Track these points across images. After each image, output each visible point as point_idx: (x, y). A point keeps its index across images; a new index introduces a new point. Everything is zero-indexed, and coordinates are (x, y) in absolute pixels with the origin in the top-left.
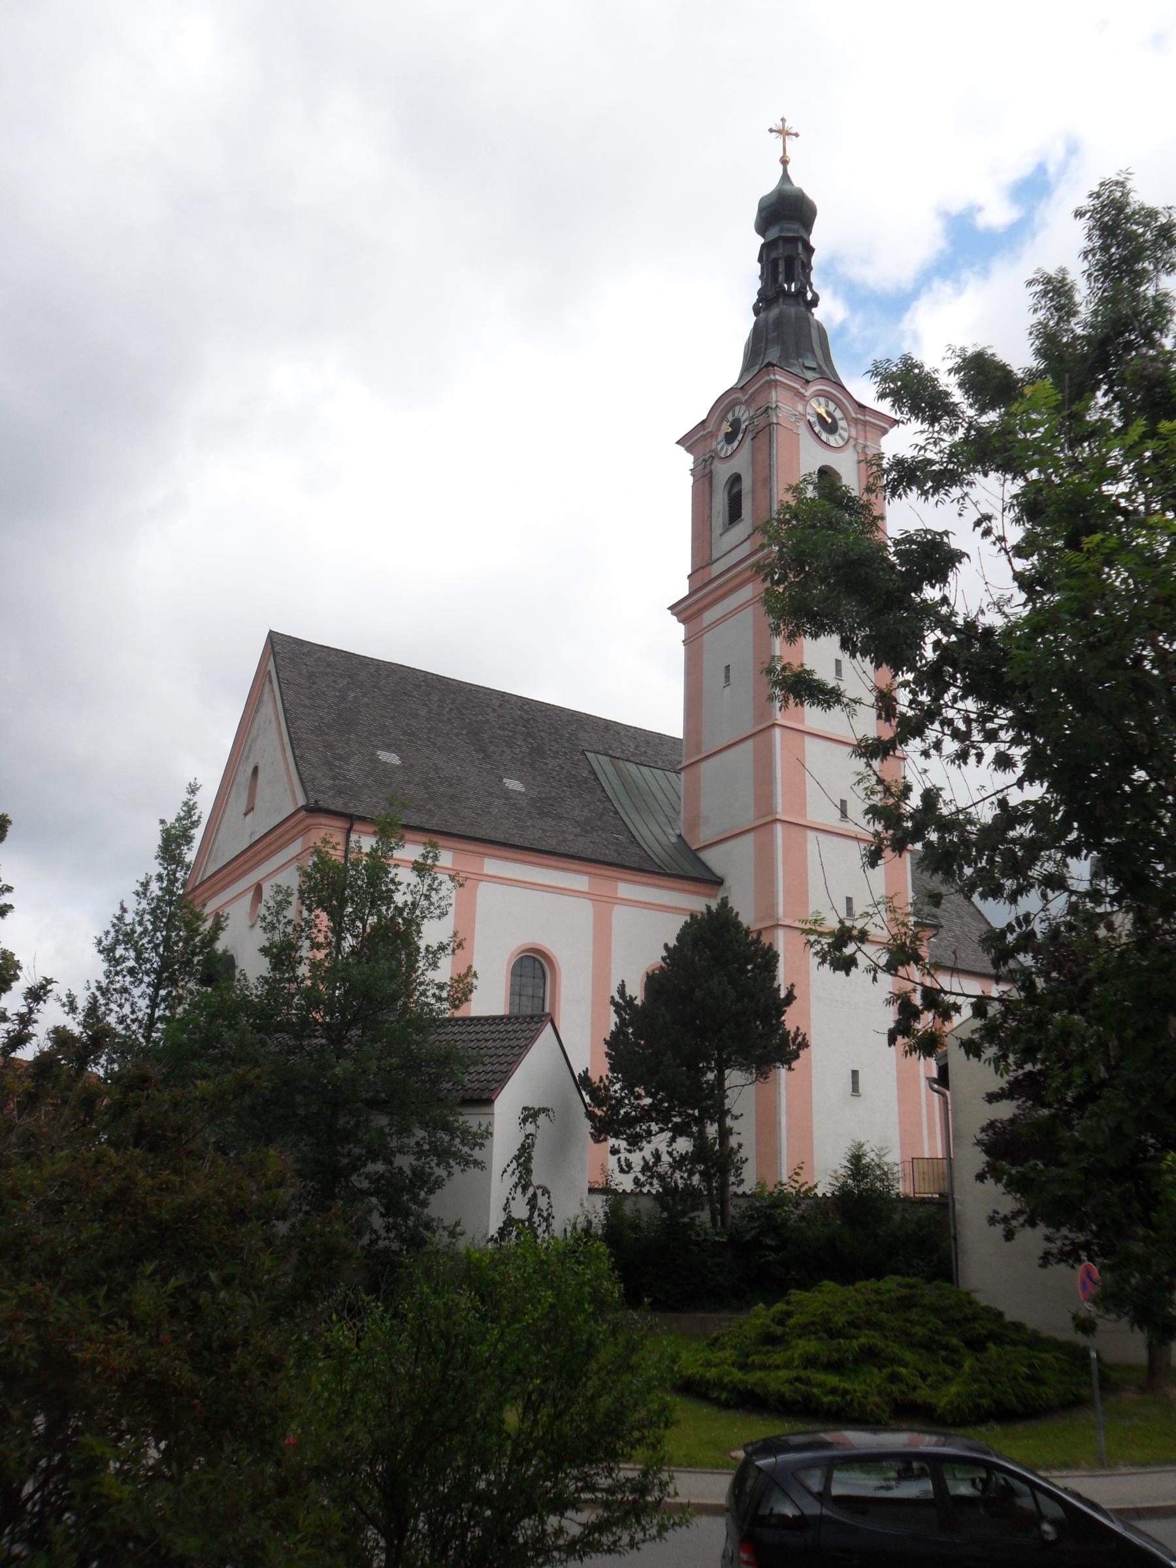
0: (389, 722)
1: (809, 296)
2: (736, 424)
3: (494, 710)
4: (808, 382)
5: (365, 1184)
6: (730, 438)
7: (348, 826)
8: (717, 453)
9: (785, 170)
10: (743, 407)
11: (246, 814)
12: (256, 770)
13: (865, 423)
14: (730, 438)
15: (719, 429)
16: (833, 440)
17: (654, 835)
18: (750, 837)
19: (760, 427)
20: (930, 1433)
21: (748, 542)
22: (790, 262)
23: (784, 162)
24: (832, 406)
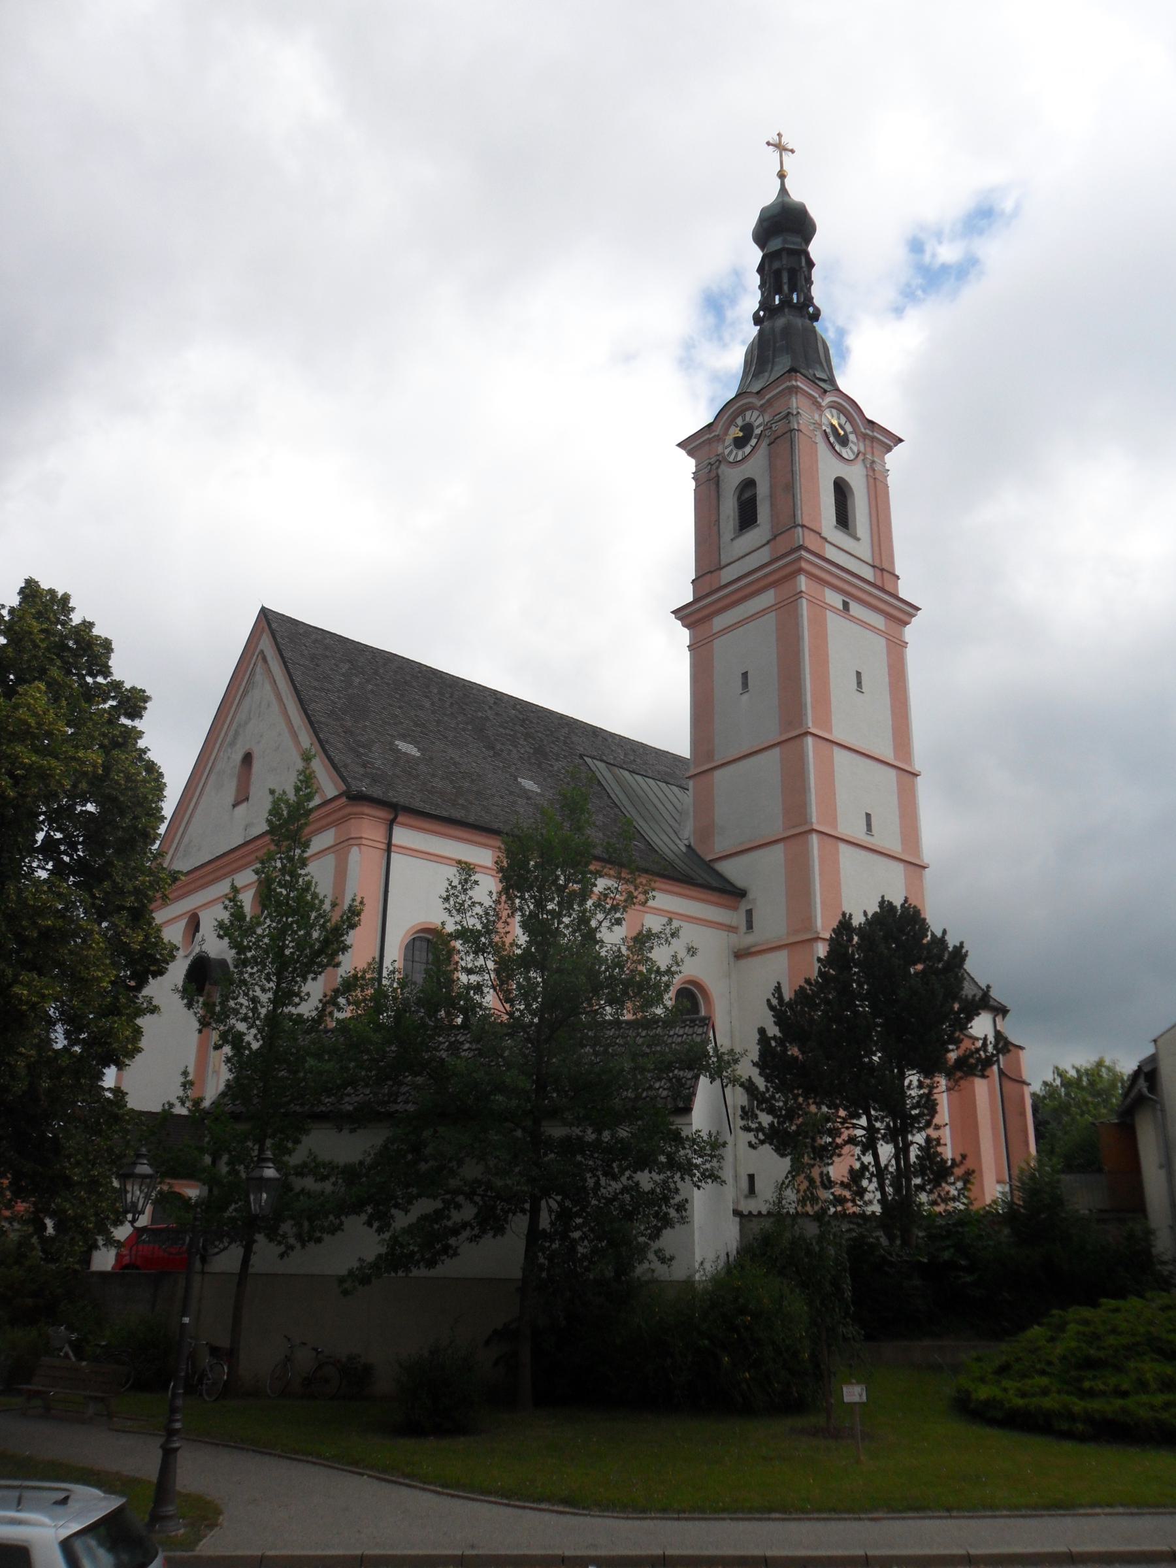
0: (398, 712)
2: (748, 429)
3: (491, 708)
4: (825, 391)
5: (457, 1217)
6: (740, 443)
7: (392, 817)
8: (725, 459)
9: (783, 184)
10: (756, 413)
11: (234, 806)
12: (248, 759)
13: (873, 439)
14: (740, 443)
16: (845, 452)
17: (670, 843)
18: (780, 847)
19: (779, 433)
21: (766, 548)
23: (782, 176)
24: (843, 420)
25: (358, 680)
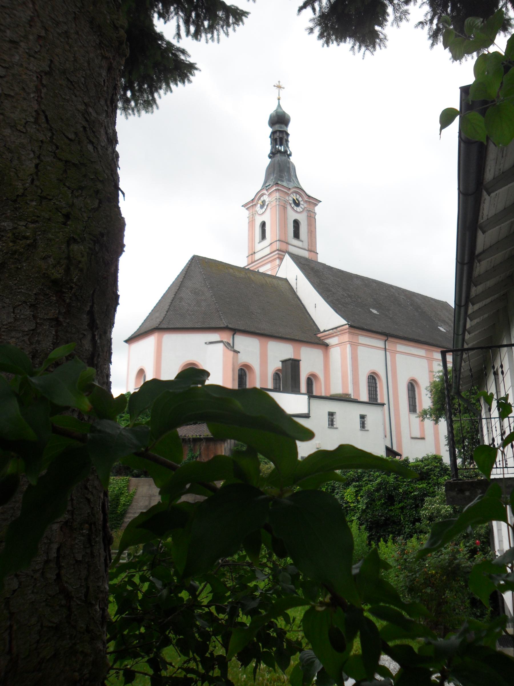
1: (289, 153)
13: (310, 202)
15: (258, 203)
16: (299, 209)
20: (264, 275)
21: (269, 247)
22: (281, 139)
23: (279, 99)
24: (298, 196)
25: (55, 298)
